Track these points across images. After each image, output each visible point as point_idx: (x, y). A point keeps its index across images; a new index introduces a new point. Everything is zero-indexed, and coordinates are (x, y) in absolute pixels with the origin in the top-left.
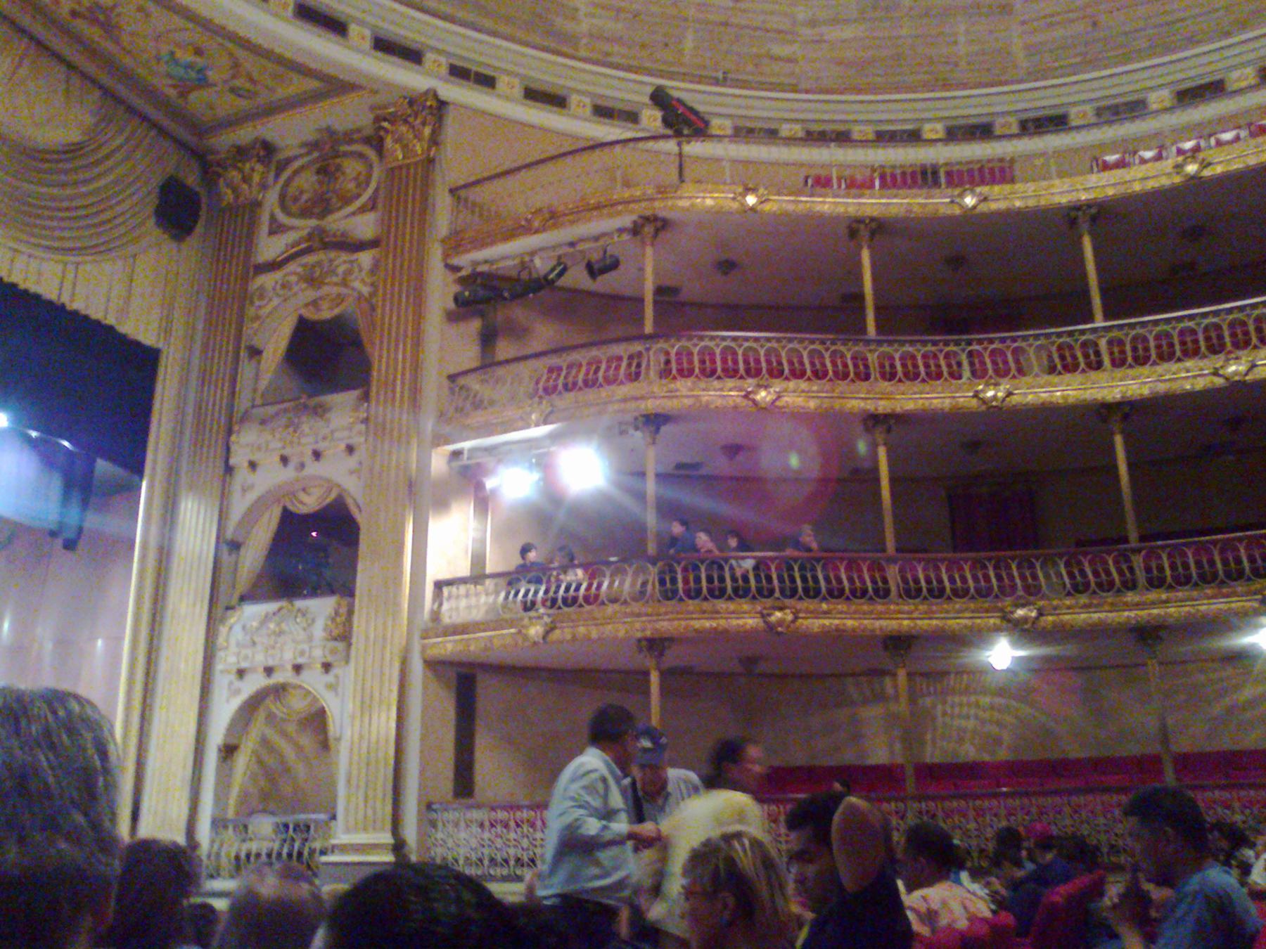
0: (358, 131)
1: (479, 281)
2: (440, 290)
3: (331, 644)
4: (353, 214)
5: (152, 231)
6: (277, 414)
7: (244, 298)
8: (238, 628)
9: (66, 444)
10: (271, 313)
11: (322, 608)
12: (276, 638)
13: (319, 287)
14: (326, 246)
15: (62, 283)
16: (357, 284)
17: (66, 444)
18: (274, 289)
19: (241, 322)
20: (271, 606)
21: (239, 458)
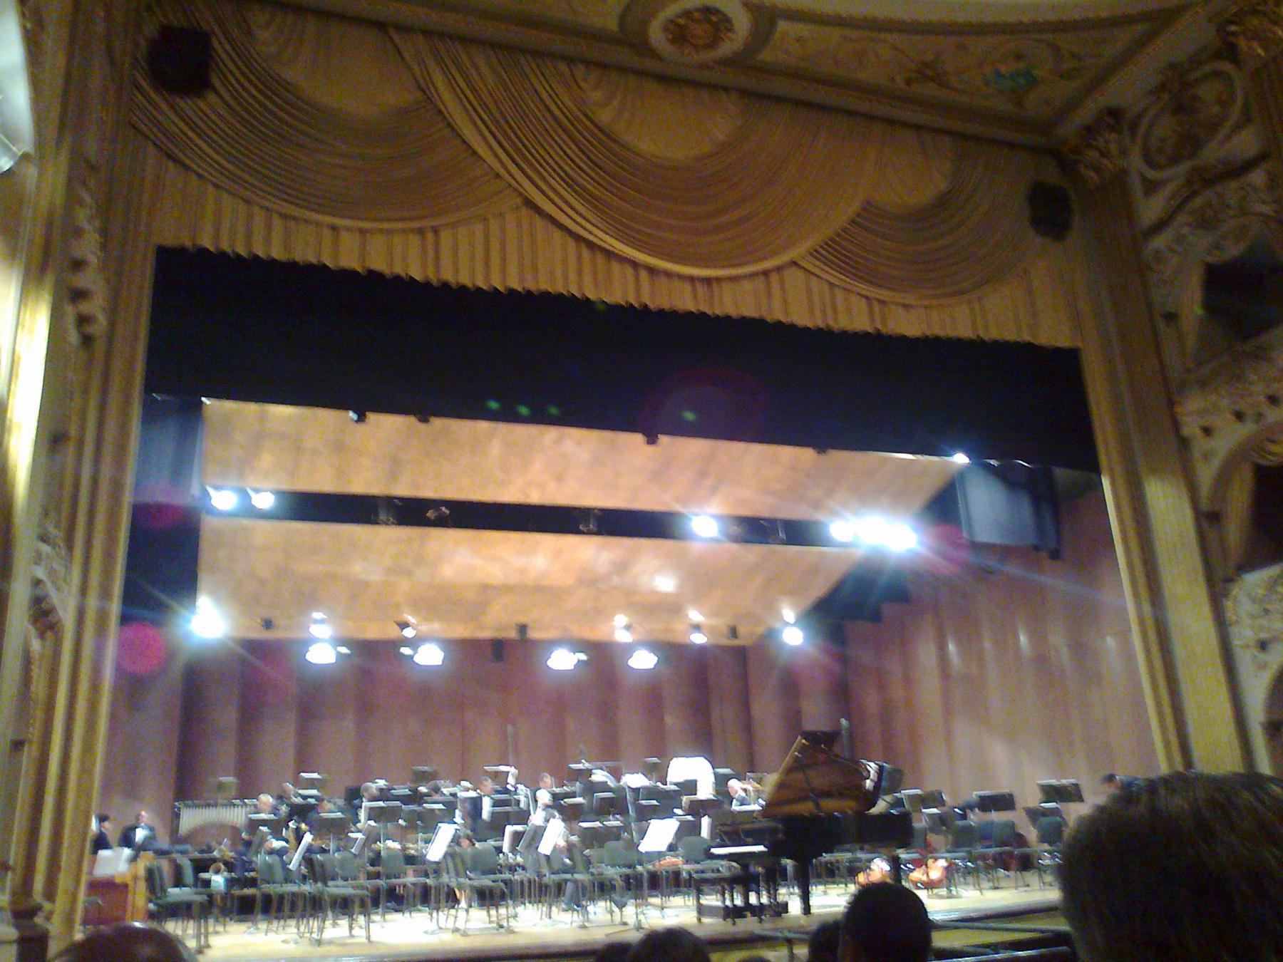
5: (1034, 240)
14: (1208, 183)
21: (1191, 428)
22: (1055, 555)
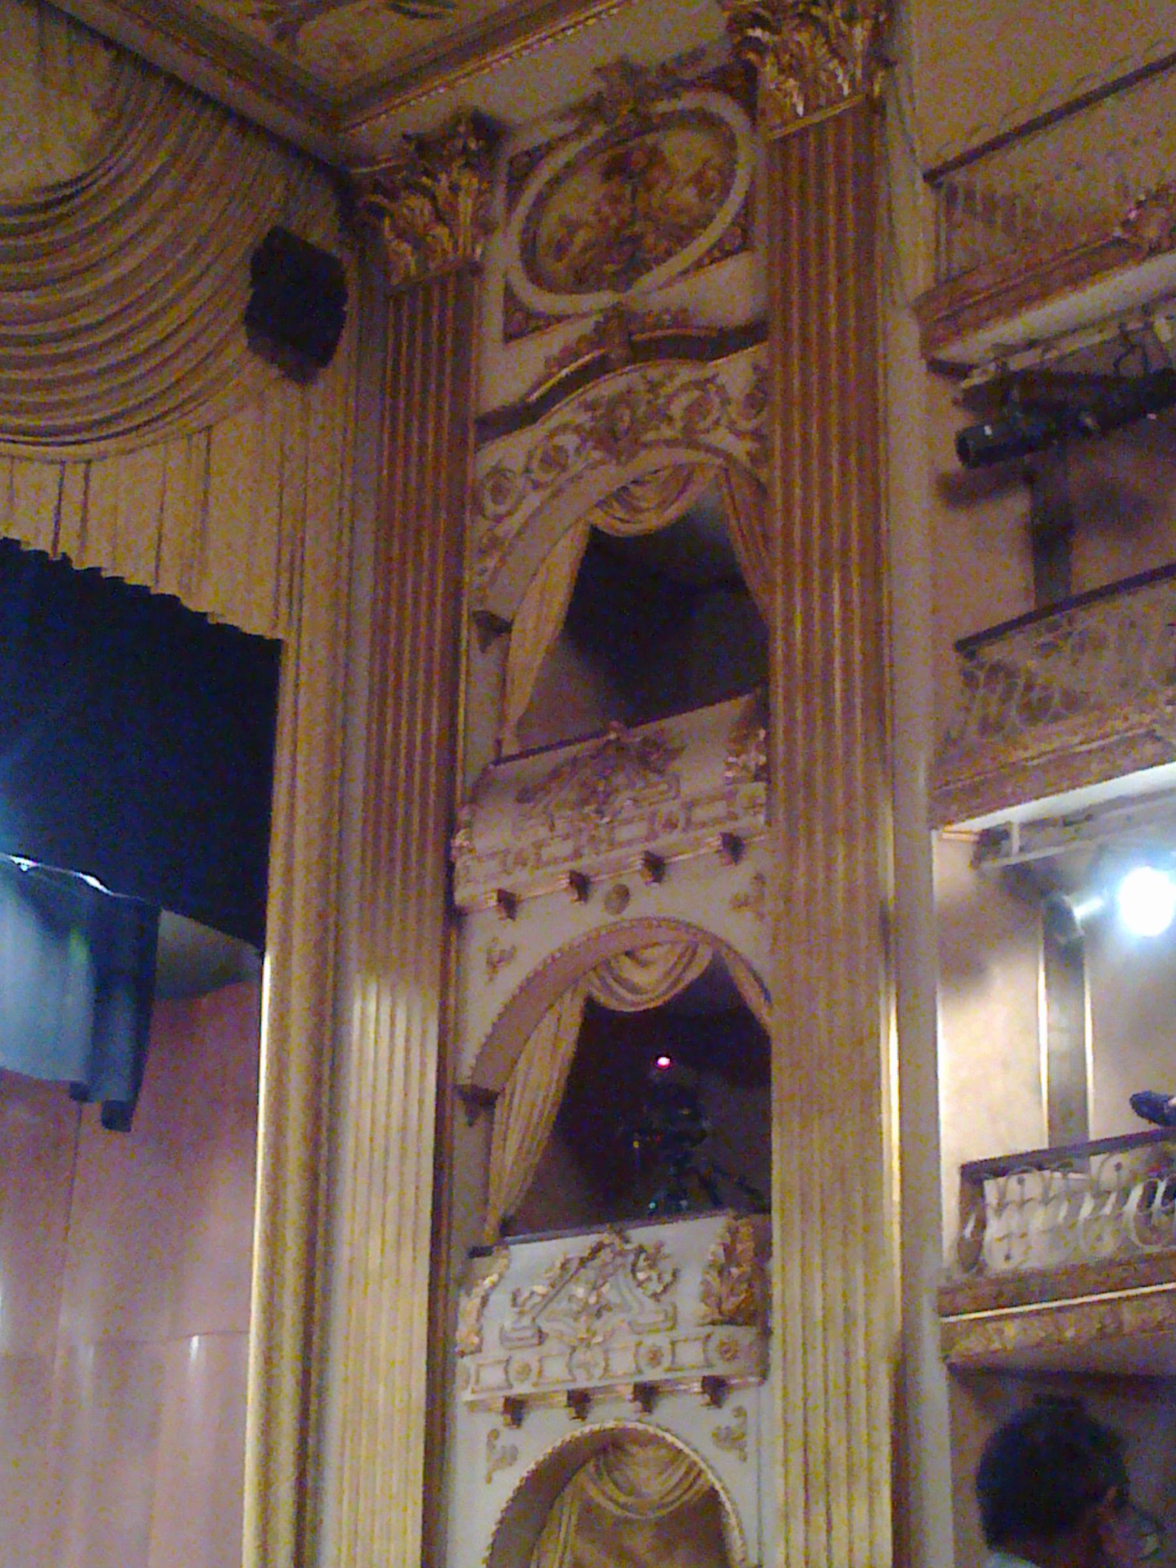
0: (696, 56)
1: (1016, 394)
2: (921, 428)
3: (722, 1333)
4: (699, 265)
5: (240, 362)
6: (555, 774)
7: (462, 500)
8: (500, 1299)
9: (92, 881)
10: (525, 525)
11: (692, 1242)
12: (590, 1320)
13: (632, 456)
14: (646, 350)
15: (58, 513)
16: (722, 438)
17: (92, 881)
18: (527, 470)
19: (456, 553)
20: (576, 1245)
21: (476, 888)
22: (117, 1118)
